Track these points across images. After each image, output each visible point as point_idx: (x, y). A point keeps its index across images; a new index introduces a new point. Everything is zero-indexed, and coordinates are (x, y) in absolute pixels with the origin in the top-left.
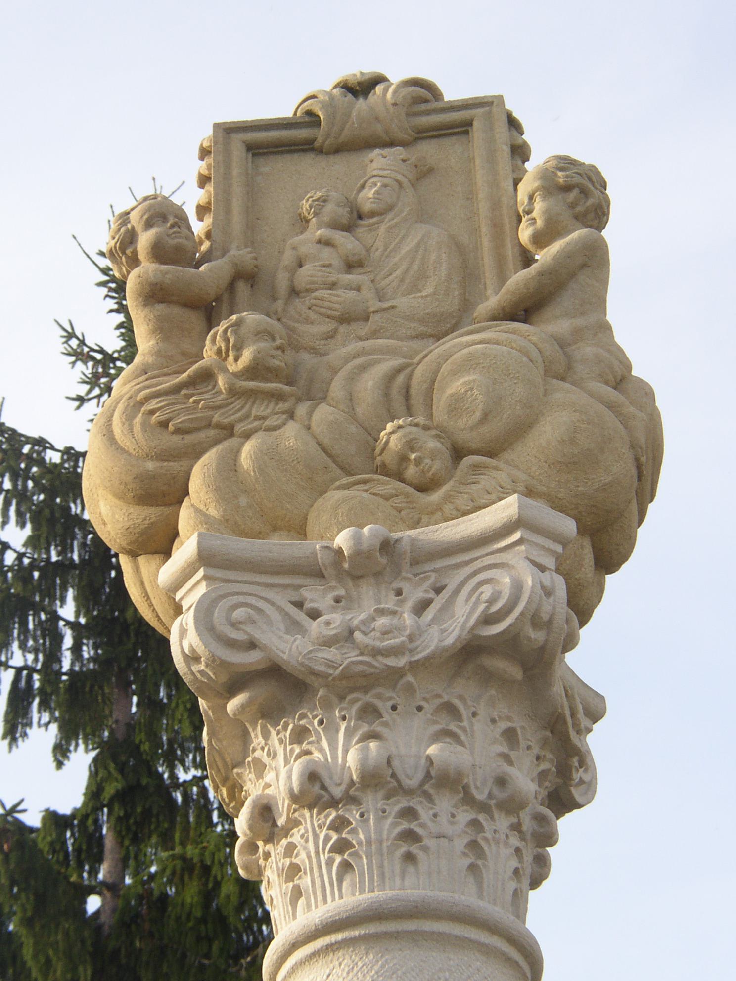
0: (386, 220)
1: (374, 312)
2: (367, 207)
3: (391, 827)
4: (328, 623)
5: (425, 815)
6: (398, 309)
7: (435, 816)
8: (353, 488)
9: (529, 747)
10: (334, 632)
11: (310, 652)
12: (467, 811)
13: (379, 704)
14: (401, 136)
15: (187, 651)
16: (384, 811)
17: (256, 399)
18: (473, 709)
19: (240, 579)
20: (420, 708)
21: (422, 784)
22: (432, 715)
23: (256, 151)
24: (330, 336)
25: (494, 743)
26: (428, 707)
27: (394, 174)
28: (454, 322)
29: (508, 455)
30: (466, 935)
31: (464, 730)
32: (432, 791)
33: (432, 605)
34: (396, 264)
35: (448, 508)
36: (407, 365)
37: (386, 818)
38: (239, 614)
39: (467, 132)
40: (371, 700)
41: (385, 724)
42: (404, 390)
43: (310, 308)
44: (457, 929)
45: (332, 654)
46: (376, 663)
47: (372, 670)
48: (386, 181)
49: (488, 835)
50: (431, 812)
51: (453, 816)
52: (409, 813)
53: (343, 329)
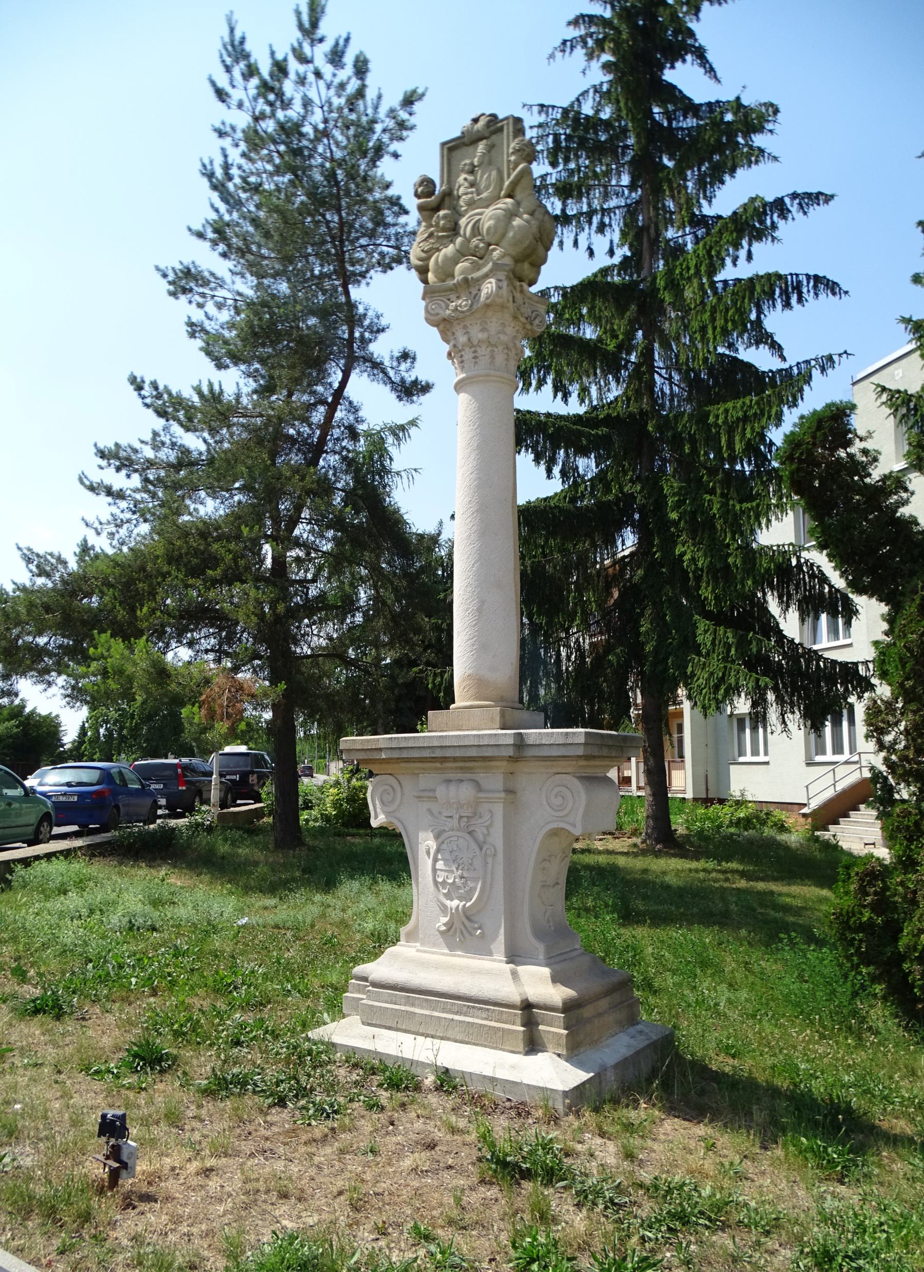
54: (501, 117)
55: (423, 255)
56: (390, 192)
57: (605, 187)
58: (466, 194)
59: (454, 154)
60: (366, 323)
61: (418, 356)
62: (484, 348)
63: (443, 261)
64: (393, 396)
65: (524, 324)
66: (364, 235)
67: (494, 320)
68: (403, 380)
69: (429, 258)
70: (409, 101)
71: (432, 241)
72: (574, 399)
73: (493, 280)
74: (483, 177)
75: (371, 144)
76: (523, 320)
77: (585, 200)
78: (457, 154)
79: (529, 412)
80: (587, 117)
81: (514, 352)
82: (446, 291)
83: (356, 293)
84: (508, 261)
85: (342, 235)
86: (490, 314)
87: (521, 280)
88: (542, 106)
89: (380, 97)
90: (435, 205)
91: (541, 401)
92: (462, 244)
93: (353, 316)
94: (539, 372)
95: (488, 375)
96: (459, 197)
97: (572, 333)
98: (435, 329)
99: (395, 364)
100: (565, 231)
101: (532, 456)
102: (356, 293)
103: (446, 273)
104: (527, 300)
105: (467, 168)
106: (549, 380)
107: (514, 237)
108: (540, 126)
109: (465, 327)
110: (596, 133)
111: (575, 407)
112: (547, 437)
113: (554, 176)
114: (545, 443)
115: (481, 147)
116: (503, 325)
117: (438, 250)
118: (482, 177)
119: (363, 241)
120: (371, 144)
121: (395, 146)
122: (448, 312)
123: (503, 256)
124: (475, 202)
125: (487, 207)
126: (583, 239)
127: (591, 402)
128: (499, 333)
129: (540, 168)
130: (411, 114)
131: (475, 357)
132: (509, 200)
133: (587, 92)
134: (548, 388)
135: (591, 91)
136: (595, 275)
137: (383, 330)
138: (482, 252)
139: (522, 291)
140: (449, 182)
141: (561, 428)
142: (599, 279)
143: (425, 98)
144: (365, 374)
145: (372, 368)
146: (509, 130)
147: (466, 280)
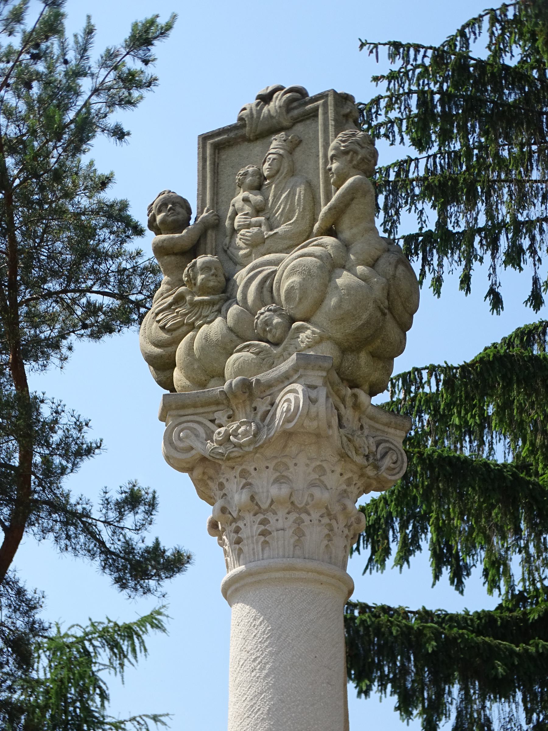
3: (257, 529)
14: (286, 123)
19: (187, 413)
20: (267, 467)
35: (285, 354)
54: (312, 93)
55: (164, 336)
56: (110, 195)
57: (520, 183)
58: (248, 226)
59: (224, 155)
60: (55, 438)
61: (160, 500)
62: (281, 513)
63: (202, 349)
64: (108, 579)
65: (362, 468)
66: (55, 274)
67: (302, 459)
68: (129, 548)
69: (176, 342)
70: (143, 38)
71: (181, 310)
72: (475, 580)
73: (298, 387)
74: (279, 198)
75: (71, 115)
76: (359, 460)
77: (481, 207)
78: (230, 156)
79: (386, 609)
80: (480, 64)
81: (342, 520)
82: (208, 404)
83: (40, 380)
84: (327, 350)
85: (14, 273)
86: (293, 448)
87: (353, 385)
88: (396, 45)
89: (90, 31)
90: (187, 244)
91: (408, 585)
92: (238, 318)
93: (30, 426)
94: (404, 526)
95: (292, 568)
96: (234, 232)
97: (467, 453)
98: (186, 475)
99: (112, 515)
100: (445, 261)
101: (394, 700)
102: (40, 380)
103: (208, 370)
104: (366, 421)
105: (248, 180)
106: (425, 544)
107: (339, 305)
108: (392, 76)
109: (244, 474)
110: (498, 89)
111: (477, 597)
112: (424, 659)
113: (422, 164)
114: (419, 672)
115: (276, 144)
116: (321, 470)
117: (193, 327)
118: (277, 197)
119: (53, 285)
120: (71, 115)
121: (118, 117)
122: (210, 445)
123: (320, 340)
124: (264, 241)
125: (288, 250)
126: (480, 273)
127: (511, 587)
128: (312, 485)
129: (390, 152)
130: (146, 62)
131: (263, 533)
132: (328, 240)
133: (478, 20)
134: (423, 558)
135: (486, 19)
136: (508, 342)
137: (89, 451)
138: (278, 333)
139: (356, 406)
140: (215, 203)
141: (451, 641)
142: (516, 351)
143: (172, 33)
144: (51, 536)
145: (66, 524)
146: (328, 115)
147: (246, 385)
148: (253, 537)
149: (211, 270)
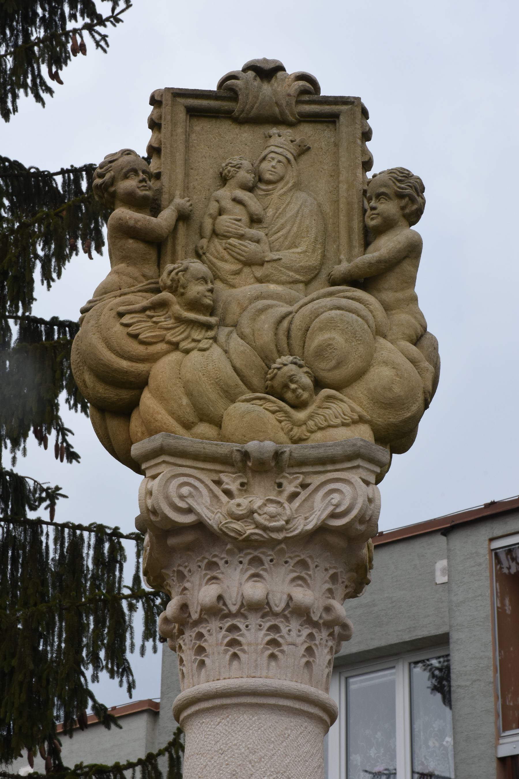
0: (278, 188)
1: (267, 262)
2: (268, 176)
4: (239, 505)
5: (284, 630)
6: (283, 261)
7: (290, 631)
8: (252, 402)
9: (343, 582)
10: (241, 513)
11: (226, 523)
12: (307, 628)
13: (263, 557)
15: (150, 508)
16: (260, 626)
17: (194, 326)
18: (316, 563)
19: (184, 464)
20: (286, 562)
21: (284, 610)
22: (293, 567)
23: (193, 114)
24: (237, 273)
25: (325, 582)
26: (292, 562)
27: (286, 153)
28: (316, 272)
29: (348, 390)
30: (302, 708)
31: (310, 576)
32: (289, 615)
33: (300, 496)
34: (282, 225)
36: (290, 313)
37: (261, 630)
38: (185, 490)
39: (334, 122)
40: (259, 555)
41: (265, 570)
42: (286, 333)
43: (225, 249)
44: (297, 705)
45: (237, 526)
46: (265, 535)
47: (262, 539)
48: (281, 158)
49: (317, 642)
50: (288, 628)
51: (299, 631)
52: (274, 628)
53: (246, 270)
148: (257, 645)
149: (206, 283)
